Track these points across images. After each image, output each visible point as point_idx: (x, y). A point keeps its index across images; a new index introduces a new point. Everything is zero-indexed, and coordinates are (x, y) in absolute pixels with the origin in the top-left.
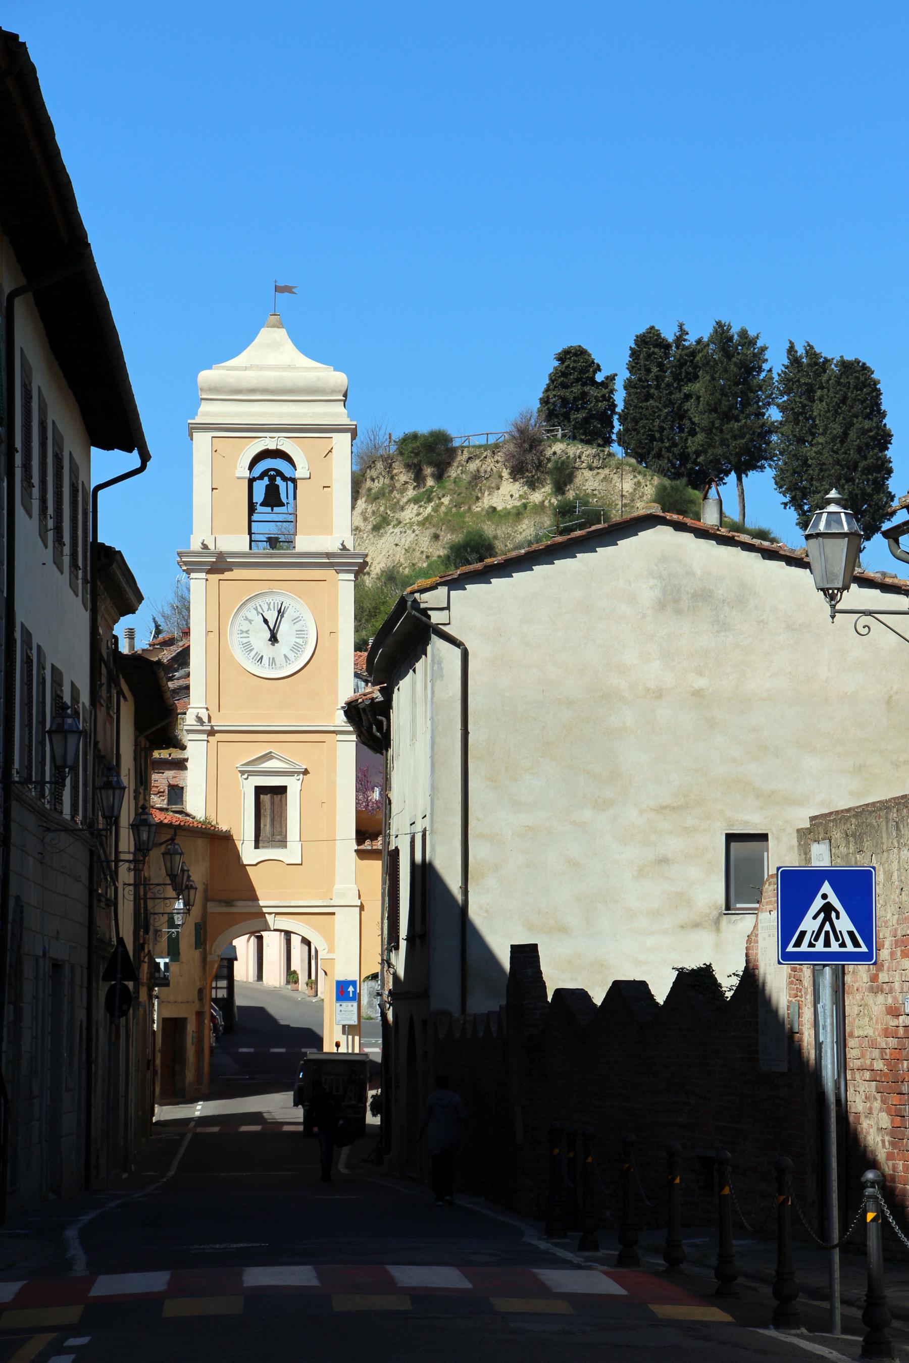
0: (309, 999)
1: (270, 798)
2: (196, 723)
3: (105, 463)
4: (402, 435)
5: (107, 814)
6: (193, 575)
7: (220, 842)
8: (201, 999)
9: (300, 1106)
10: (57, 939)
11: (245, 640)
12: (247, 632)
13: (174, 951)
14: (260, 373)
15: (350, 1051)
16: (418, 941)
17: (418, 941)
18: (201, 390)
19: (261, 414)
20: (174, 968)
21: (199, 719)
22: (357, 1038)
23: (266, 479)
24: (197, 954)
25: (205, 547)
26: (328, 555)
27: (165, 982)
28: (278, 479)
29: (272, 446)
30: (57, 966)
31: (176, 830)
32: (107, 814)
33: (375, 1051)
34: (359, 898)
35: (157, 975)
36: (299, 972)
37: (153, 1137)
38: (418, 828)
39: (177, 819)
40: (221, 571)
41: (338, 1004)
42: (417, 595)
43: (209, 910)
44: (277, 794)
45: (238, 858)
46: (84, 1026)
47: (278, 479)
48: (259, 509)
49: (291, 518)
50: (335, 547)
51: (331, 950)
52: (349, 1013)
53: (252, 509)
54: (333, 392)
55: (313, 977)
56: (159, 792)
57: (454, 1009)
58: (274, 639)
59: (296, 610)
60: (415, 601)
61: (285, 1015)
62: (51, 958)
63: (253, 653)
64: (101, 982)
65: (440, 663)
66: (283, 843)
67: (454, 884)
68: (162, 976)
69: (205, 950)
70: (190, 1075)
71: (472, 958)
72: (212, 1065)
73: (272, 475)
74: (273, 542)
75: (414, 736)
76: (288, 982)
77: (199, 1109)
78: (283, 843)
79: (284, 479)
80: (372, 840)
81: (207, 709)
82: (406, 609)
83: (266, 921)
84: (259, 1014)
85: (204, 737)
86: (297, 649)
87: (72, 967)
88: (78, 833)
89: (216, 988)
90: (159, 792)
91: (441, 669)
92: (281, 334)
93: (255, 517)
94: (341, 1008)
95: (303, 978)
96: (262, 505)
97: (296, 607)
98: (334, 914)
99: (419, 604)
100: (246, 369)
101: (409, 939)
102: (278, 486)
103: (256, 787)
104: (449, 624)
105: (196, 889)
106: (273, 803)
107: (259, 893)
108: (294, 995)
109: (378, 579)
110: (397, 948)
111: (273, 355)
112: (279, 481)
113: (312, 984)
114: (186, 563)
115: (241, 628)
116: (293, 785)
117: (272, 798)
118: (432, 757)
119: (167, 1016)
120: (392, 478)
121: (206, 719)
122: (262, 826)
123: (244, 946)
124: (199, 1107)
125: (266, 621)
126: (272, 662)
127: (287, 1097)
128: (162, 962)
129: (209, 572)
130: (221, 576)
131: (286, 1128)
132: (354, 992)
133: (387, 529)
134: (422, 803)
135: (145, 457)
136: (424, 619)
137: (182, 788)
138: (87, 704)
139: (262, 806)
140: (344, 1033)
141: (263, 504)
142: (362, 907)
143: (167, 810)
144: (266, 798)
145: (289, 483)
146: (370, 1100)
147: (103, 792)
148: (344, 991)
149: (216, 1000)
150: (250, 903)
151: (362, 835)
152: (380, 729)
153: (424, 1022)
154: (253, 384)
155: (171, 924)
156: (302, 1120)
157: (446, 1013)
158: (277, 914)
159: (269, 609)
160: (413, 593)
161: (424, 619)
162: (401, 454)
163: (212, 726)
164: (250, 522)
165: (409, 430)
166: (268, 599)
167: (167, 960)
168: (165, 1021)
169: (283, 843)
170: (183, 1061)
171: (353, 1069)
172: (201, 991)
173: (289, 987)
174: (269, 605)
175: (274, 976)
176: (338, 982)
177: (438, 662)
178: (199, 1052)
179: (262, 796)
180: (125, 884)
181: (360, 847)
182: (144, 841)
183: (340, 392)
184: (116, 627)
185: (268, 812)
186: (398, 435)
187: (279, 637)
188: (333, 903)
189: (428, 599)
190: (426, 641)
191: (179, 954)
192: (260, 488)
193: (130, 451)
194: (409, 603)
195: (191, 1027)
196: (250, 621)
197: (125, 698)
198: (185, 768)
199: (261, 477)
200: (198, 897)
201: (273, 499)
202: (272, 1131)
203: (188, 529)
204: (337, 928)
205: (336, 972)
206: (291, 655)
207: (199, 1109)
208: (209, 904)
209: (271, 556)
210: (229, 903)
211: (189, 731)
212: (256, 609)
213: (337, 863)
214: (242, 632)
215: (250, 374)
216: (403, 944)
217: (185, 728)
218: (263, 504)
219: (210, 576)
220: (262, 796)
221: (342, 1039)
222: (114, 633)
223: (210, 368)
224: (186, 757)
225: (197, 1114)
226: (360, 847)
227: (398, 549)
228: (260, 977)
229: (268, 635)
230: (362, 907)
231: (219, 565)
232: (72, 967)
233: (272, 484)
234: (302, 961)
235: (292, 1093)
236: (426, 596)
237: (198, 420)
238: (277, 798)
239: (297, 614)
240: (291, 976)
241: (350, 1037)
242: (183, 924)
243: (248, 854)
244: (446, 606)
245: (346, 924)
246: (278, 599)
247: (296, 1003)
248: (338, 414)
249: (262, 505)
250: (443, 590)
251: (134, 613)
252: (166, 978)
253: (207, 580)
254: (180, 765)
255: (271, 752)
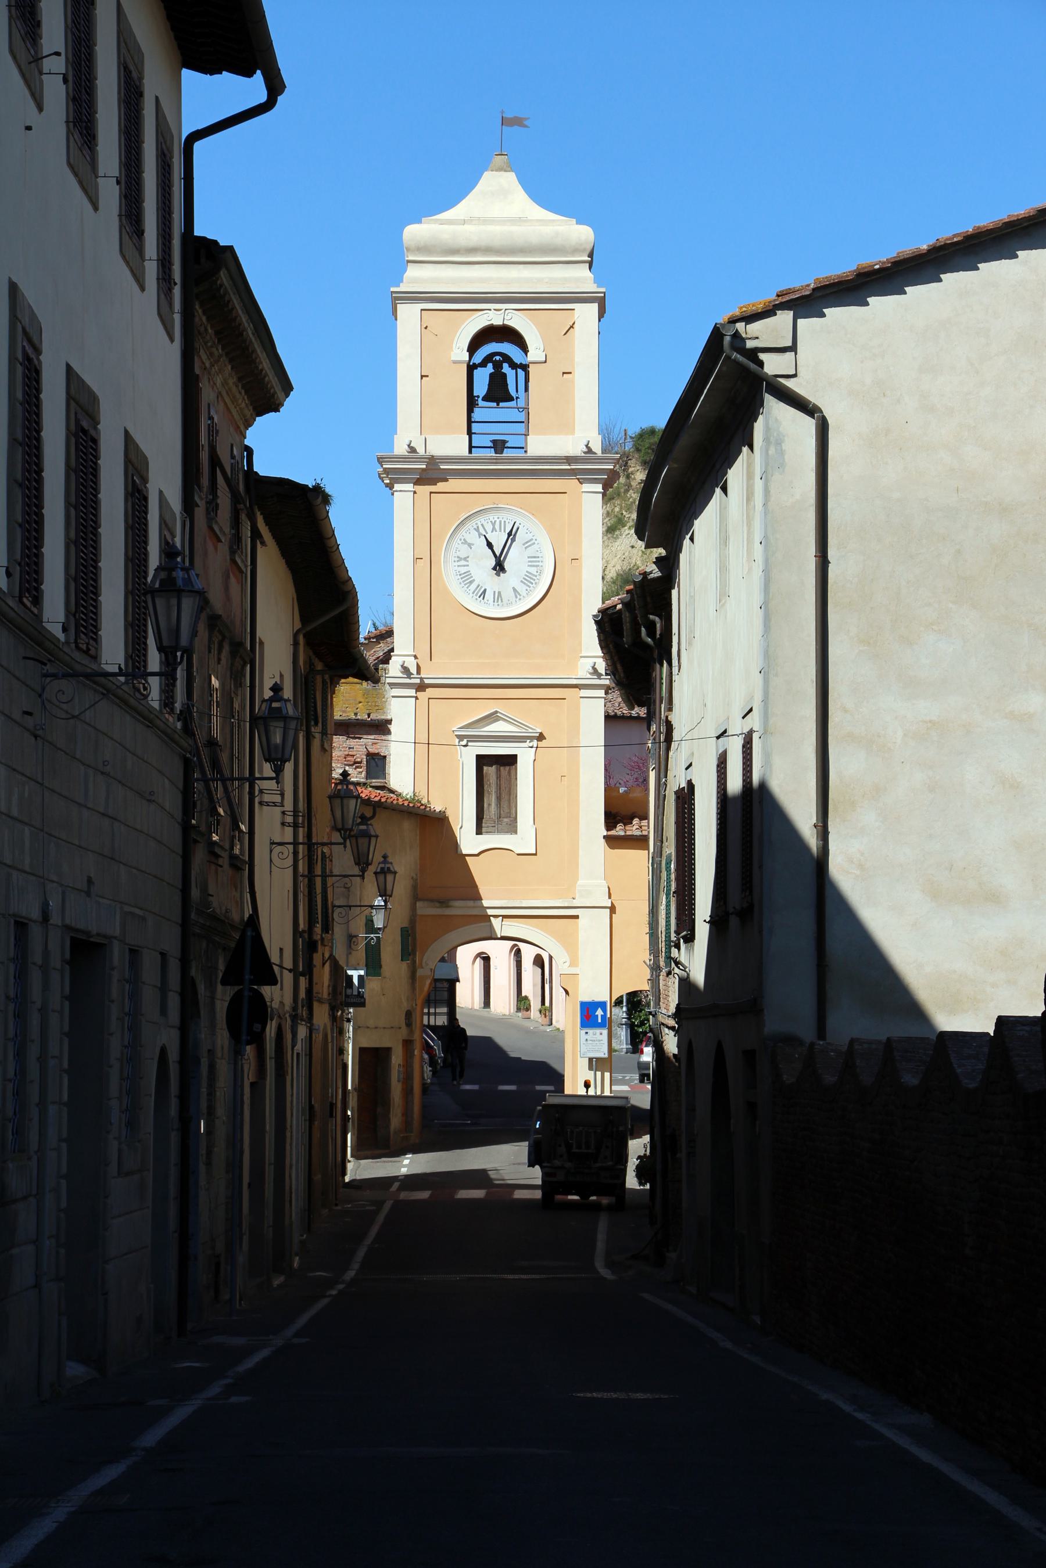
0: (542, 1028)
1: (495, 771)
2: (401, 675)
3: (207, 95)
4: (638, 430)
5: (165, 643)
6: (397, 487)
7: (432, 825)
8: (409, 1024)
9: (537, 1167)
10: (88, 894)
11: (463, 570)
12: (465, 559)
13: (373, 964)
14: (482, 227)
15: (599, 1093)
16: (734, 921)
17: (734, 921)
18: (408, 249)
19: (482, 280)
20: (373, 985)
21: (406, 670)
22: (607, 1075)
23: (490, 365)
24: (404, 966)
25: (413, 450)
26: (569, 460)
27: (359, 1001)
28: (505, 366)
29: (498, 321)
30: (85, 950)
31: (377, 806)
32: (165, 643)
33: (642, 1098)
34: (610, 897)
35: (349, 991)
36: (531, 998)
37: (339, 1208)
38: (738, 727)
39: (375, 795)
40: (433, 482)
41: (583, 1032)
42: (740, 326)
43: (419, 912)
44: (504, 765)
45: (456, 845)
46: (173, 1055)
47: (505, 366)
48: (481, 403)
49: (522, 417)
50: (576, 449)
51: (574, 963)
52: (597, 1042)
53: (472, 403)
54: (576, 251)
55: (547, 1003)
56: (356, 763)
57: (806, 1032)
58: (499, 567)
59: (529, 532)
60: (736, 335)
61: (516, 1046)
62: (68, 928)
63: (473, 587)
64: (220, 987)
65: (779, 443)
66: (512, 828)
67: (803, 818)
68: (355, 993)
69: (414, 962)
70: (396, 1121)
71: (835, 945)
72: (424, 1107)
73: (497, 361)
74: (499, 446)
75: (723, 594)
76: (518, 1009)
77: (407, 1165)
78: (512, 829)
79: (514, 366)
80: (625, 825)
81: (416, 657)
82: (722, 351)
83: (491, 926)
84: (487, 1044)
85: (412, 692)
86: (529, 580)
87: (134, 953)
88: (102, 680)
89: (435, 1014)
90: (356, 763)
91: (781, 453)
92: (509, 179)
93: (477, 414)
94: (587, 1037)
95: (535, 1004)
96: (485, 399)
97: (531, 528)
98: (577, 917)
99: (743, 340)
100: (464, 222)
101: (717, 922)
102: (505, 375)
103: (478, 756)
104: (795, 376)
105: (395, 873)
106: (499, 777)
107: (483, 890)
108: (526, 1024)
109: (614, 583)
110: (690, 939)
111: (499, 205)
112: (506, 368)
113: (546, 1011)
114: (387, 471)
115: (458, 554)
116: (525, 756)
117: (498, 771)
118: (765, 606)
119: (365, 1044)
120: (628, 477)
121: (414, 670)
122: (486, 805)
123: (466, 956)
124: (406, 1162)
125: (490, 545)
126: (498, 597)
127: (520, 1150)
128: (355, 974)
129: (418, 482)
130: (433, 488)
131: (519, 1194)
132: (604, 1017)
133: (623, 530)
134: (743, 685)
135: (275, 87)
136: (753, 366)
137: (385, 757)
138: (175, 502)
139: (485, 780)
140: (590, 1068)
141: (486, 398)
142: (612, 909)
143: (365, 784)
144: (490, 771)
145: (519, 370)
146: (632, 1163)
147: (160, 602)
148: (589, 1014)
149: (434, 1029)
150: (471, 903)
151: (612, 818)
152: (651, 633)
153: (750, 1056)
154: (474, 241)
155: (370, 926)
156: (539, 1182)
157: (791, 1040)
158: (504, 917)
159: (494, 529)
160: (733, 321)
161: (753, 366)
162: (638, 450)
163: (421, 679)
164: (470, 422)
165: (646, 424)
166: (492, 517)
167: (362, 973)
168: (363, 1053)
169: (512, 828)
170: (386, 1104)
171: (610, 1120)
172: (409, 1015)
173: (520, 1014)
174: (494, 524)
175: (503, 1002)
176: (582, 1004)
177: (775, 441)
178: (408, 1092)
179: (485, 768)
180: (272, 843)
181: (610, 833)
182: (276, 746)
183: (584, 250)
184: (249, 432)
185: (493, 789)
186: (634, 430)
187: (507, 565)
188: (576, 903)
189: (760, 333)
190: (751, 410)
191: (380, 967)
192: (482, 378)
193: (249, 73)
194: (727, 339)
195: (396, 1059)
196: (470, 545)
197: (263, 543)
198: (389, 732)
199: (483, 364)
200: (401, 888)
201: (498, 392)
202: (499, 1196)
203: (391, 428)
204: (582, 936)
205: (580, 991)
206: (522, 589)
207: (407, 1165)
208: (418, 904)
209: (496, 461)
210: (444, 903)
211: (393, 685)
212: (477, 529)
213: (581, 853)
214: (460, 559)
215: (468, 228)
216: (702, 931)
217: (388, 680)
218: (486, 398)
219: (418, 488)
220: (485, 768)
221: (590, 1076)
222: (247, 442)
223: (420, 222)
224: (389, 717)
225: (404, 1171)
226: (610, 833)
227: (635, 551)
228: (487, 1003)
229: (493, 562)
230: (612, 909)
231: (430, 473)
232: (134, 953)
233: (497, 368)
234: (534, 985)
235: (527, 1143)
236: (755, 328)
237: (403, 288)
238: (504, 770)
239: (530, 536)
240: (522, 1002)
241: (599, 1074)
242: (385, 927)
243: (468, 841)
244: (789, 344)
245: (592, 928)
246: (508, 520)
247: (528, 1032)
248: (582, 279)
249: (485, 399)
250: (785, 317)
251: (277, 410)
252: (360, 996)
253: (415, 492)
254: (382, 727)
255: (496, 712)
